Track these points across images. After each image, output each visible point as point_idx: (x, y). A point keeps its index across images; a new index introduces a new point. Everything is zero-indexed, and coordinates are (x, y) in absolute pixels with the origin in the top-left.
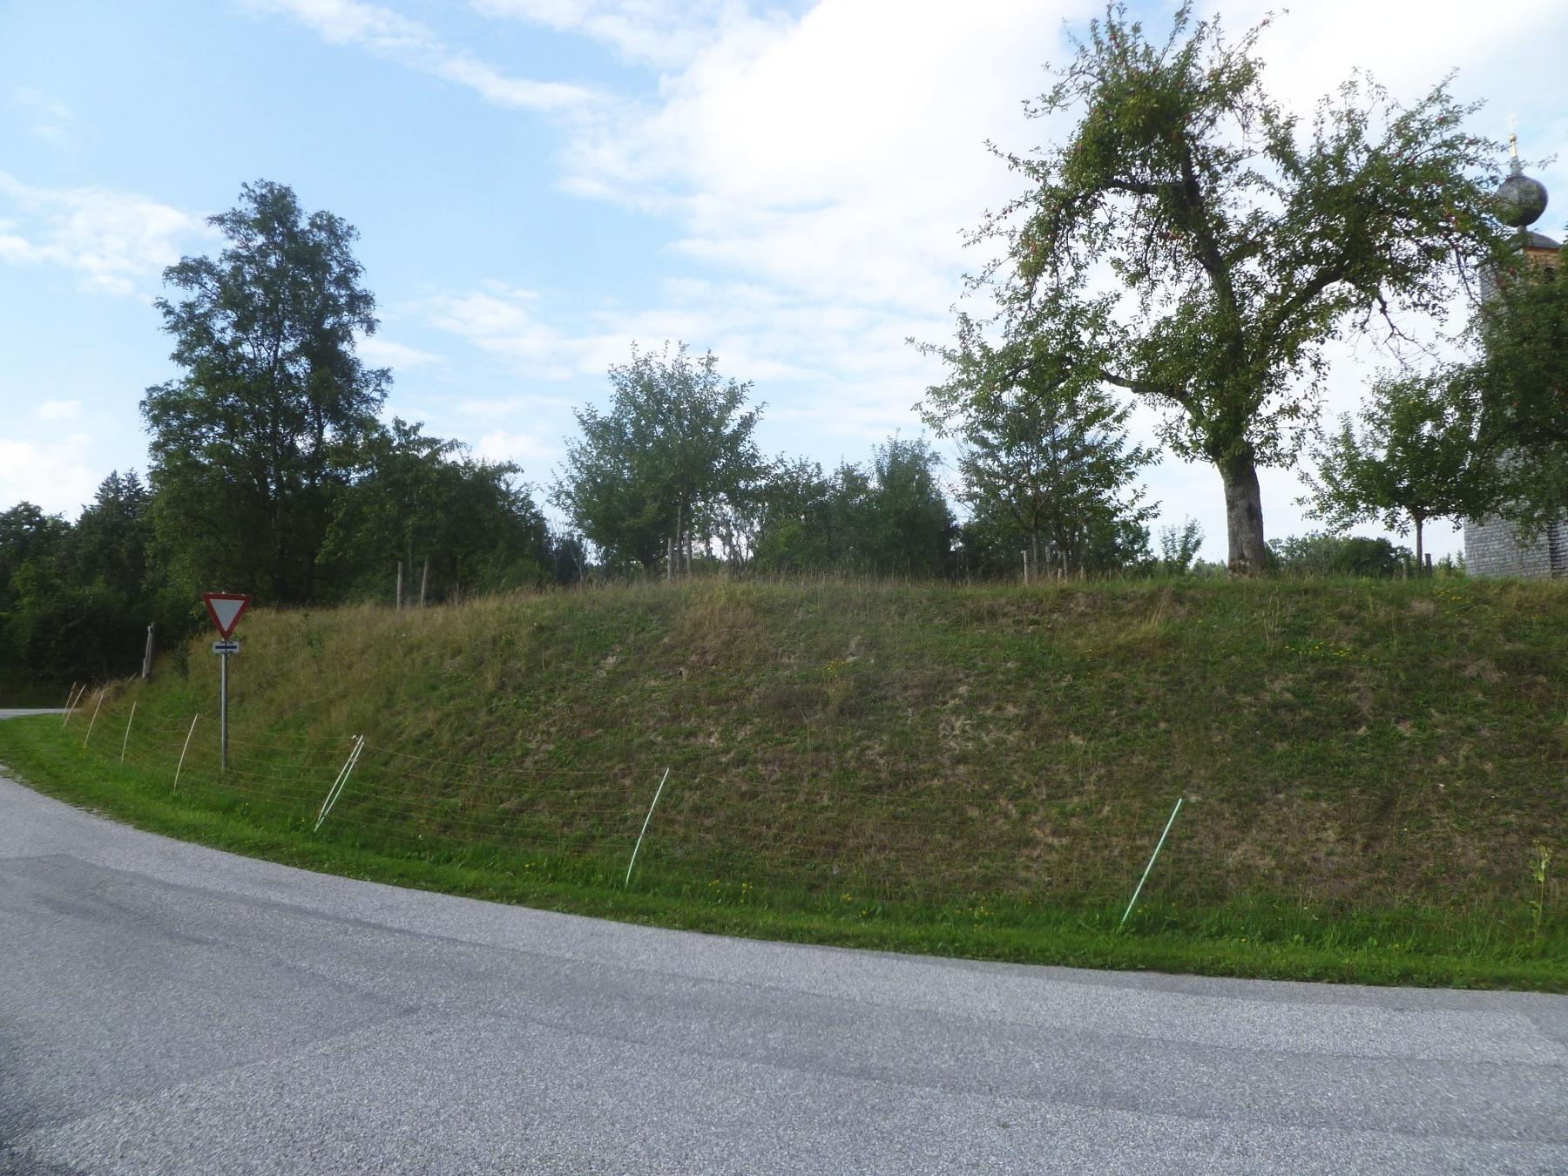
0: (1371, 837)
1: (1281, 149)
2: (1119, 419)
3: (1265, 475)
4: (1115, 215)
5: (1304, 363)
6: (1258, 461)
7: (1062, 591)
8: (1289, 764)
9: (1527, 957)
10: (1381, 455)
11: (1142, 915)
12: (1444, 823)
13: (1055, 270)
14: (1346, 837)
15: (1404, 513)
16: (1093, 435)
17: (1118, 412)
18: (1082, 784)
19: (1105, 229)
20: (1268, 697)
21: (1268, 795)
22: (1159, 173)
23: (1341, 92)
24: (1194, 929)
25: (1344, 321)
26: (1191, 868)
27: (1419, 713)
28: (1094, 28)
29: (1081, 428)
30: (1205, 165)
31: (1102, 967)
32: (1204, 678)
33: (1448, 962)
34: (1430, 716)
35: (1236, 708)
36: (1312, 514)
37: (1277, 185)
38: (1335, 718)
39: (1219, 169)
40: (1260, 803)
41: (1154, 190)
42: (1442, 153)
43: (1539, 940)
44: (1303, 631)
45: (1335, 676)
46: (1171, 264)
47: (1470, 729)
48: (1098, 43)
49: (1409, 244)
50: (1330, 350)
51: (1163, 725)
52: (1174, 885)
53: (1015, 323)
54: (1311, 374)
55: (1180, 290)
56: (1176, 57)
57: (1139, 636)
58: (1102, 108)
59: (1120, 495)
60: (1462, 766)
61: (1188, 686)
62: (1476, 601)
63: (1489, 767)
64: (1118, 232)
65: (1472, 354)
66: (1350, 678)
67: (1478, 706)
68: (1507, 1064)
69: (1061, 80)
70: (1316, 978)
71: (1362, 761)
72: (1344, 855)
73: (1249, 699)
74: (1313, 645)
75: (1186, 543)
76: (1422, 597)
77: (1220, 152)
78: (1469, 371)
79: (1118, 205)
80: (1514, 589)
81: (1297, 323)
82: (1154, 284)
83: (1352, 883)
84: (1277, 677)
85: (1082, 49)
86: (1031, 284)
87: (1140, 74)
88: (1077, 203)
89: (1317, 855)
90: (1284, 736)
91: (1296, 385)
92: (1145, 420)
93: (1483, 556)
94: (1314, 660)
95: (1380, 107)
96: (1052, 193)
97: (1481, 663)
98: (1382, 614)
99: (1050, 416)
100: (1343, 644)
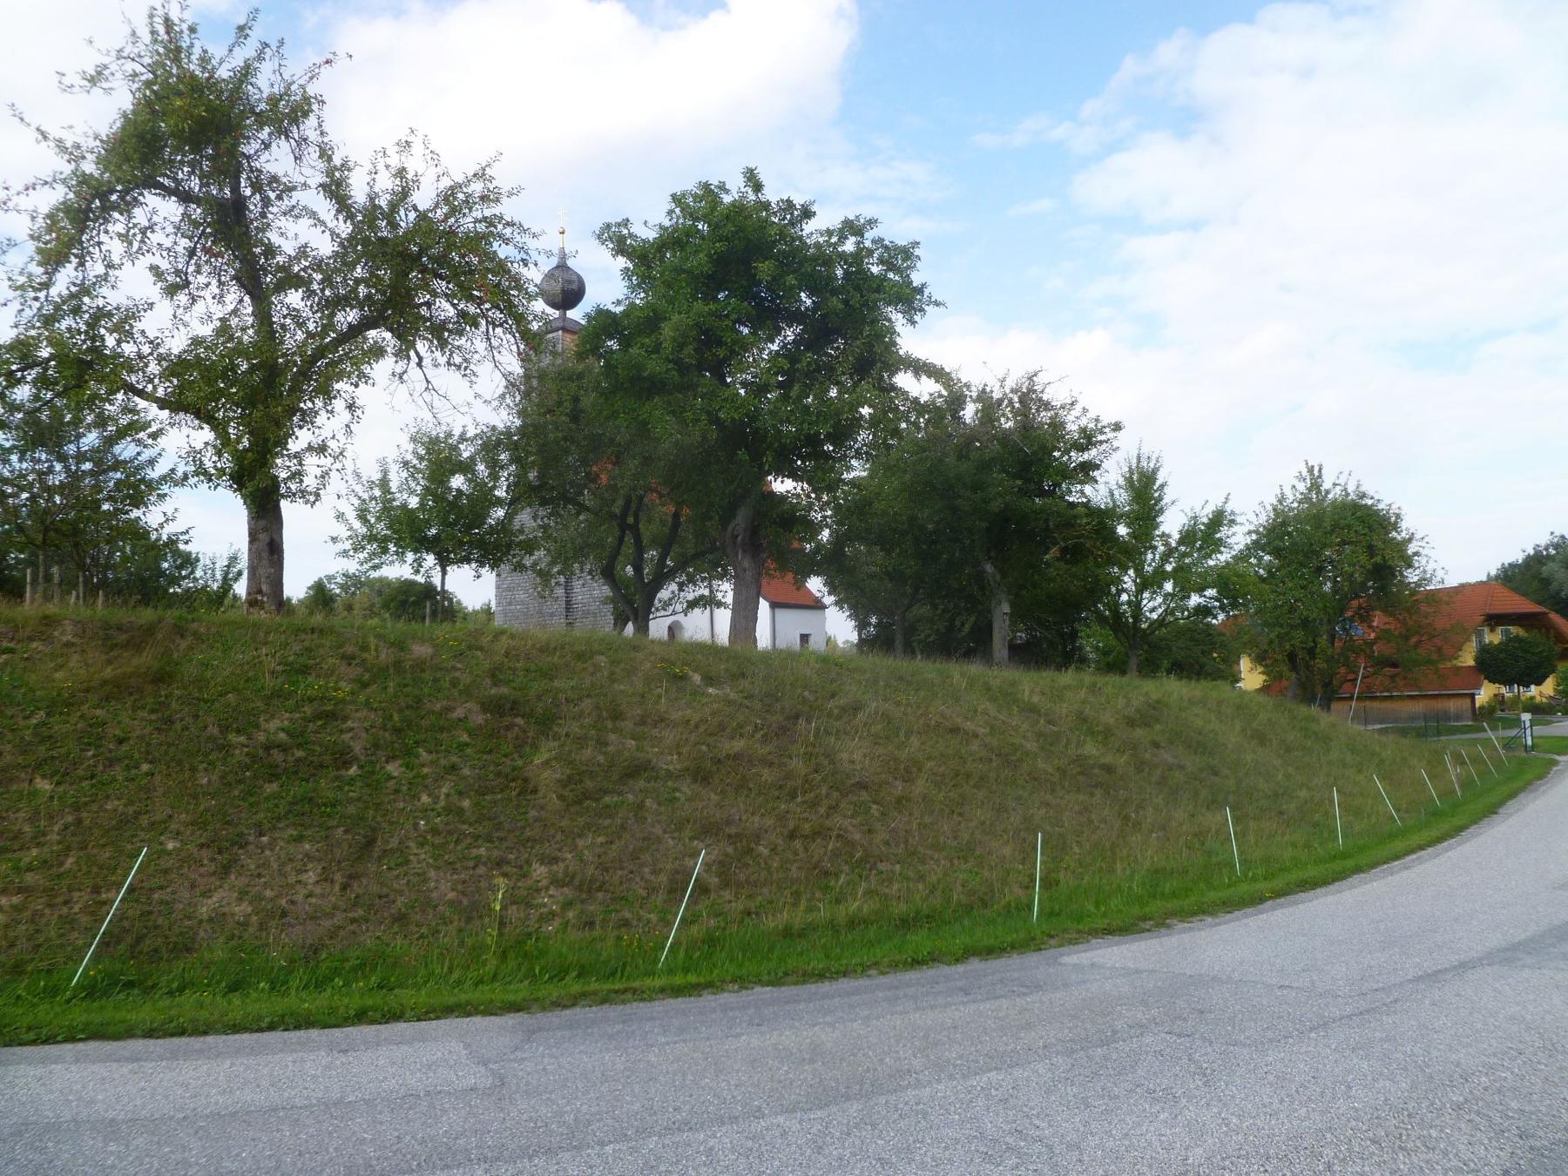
0: (351, 877)
1: (335, 189)
2: (154, 436)
3: (290, 510)
4: (155, 219)
5: (339, 404)
6: (283, 496)
7: (46, 617)
8: (277, 806)
9: (478, 983)
10: (414, 502)
11: (95, 977)
12: (420, 857)
13: (82, 264)
14: (325, 878)
15: (430, 560)
16: (126, 450)
17: (154, 428)
18: (44, 835)
19: (143, 232)
20: (261, 737)
21: (251, 839)
22: (208, 185)
23: (397, 148)
24: (153, 987)
25: (382, 369)
26: (160, 921)
27: (408, 752)
28: (151, 16)
29: (110, 441)
30: (257, 187)
31: (33, 1042)
32: (196, 717)
33: (407, 996)
34: (417, 756)
35: (226, 748)
36: (345, 553)
37: (330, 225)
38: (327, 758)
39: (272, 195)
40: (241, 847)
41: (197, 201)
42: (481, 227)
43: (491, 967)
44: (305, 671)
45: (331, 716)
46: (214, 282)
47: (454, 768)
48: (153, 32)
49: (447, 306)
50: (363, 393)
51: (145, 767)
52: (139, 939)
53: (28, 313)
54: (346, 416)
55: (219, 312)
56: (233, 70)
57: (129, 670)
58: (149, 103)
59: (151, 516)
60: (443, 803)
61: (178, 726)
62: (470, 648)
63: (466, 803)
64: (155, 238)
65: (504, 418)
66: (345, 719)
67: (462, 746)
68: (428, 1093)
69: (106, 60)
70: (272, 1027)
71: (350, 801)
72: (322, 896)
73: (242, 739)
74: (313, 685)
75: (227, 573)
76: (423, 641)
77: (274, 179)
78: (501, 433)
79: (160, 209)
80: (504, 638)
81: (333, 364)
82: (194, 300)
83: (327, 923)
84: (273, 717)
85: (134, 33)
86: (50, 274)
87: (193, 76)
88: (114, 197)
89: (295, 898)
90: (273, 777)
91: (329, 423)
92: (180, 441)
93: (510, 604)
94: (311, 700)
95: (432, 173)
96: (84, 179)
97: (468, 705)
98: (383, 656)
99: (77, 422)
100: (342, 684)
